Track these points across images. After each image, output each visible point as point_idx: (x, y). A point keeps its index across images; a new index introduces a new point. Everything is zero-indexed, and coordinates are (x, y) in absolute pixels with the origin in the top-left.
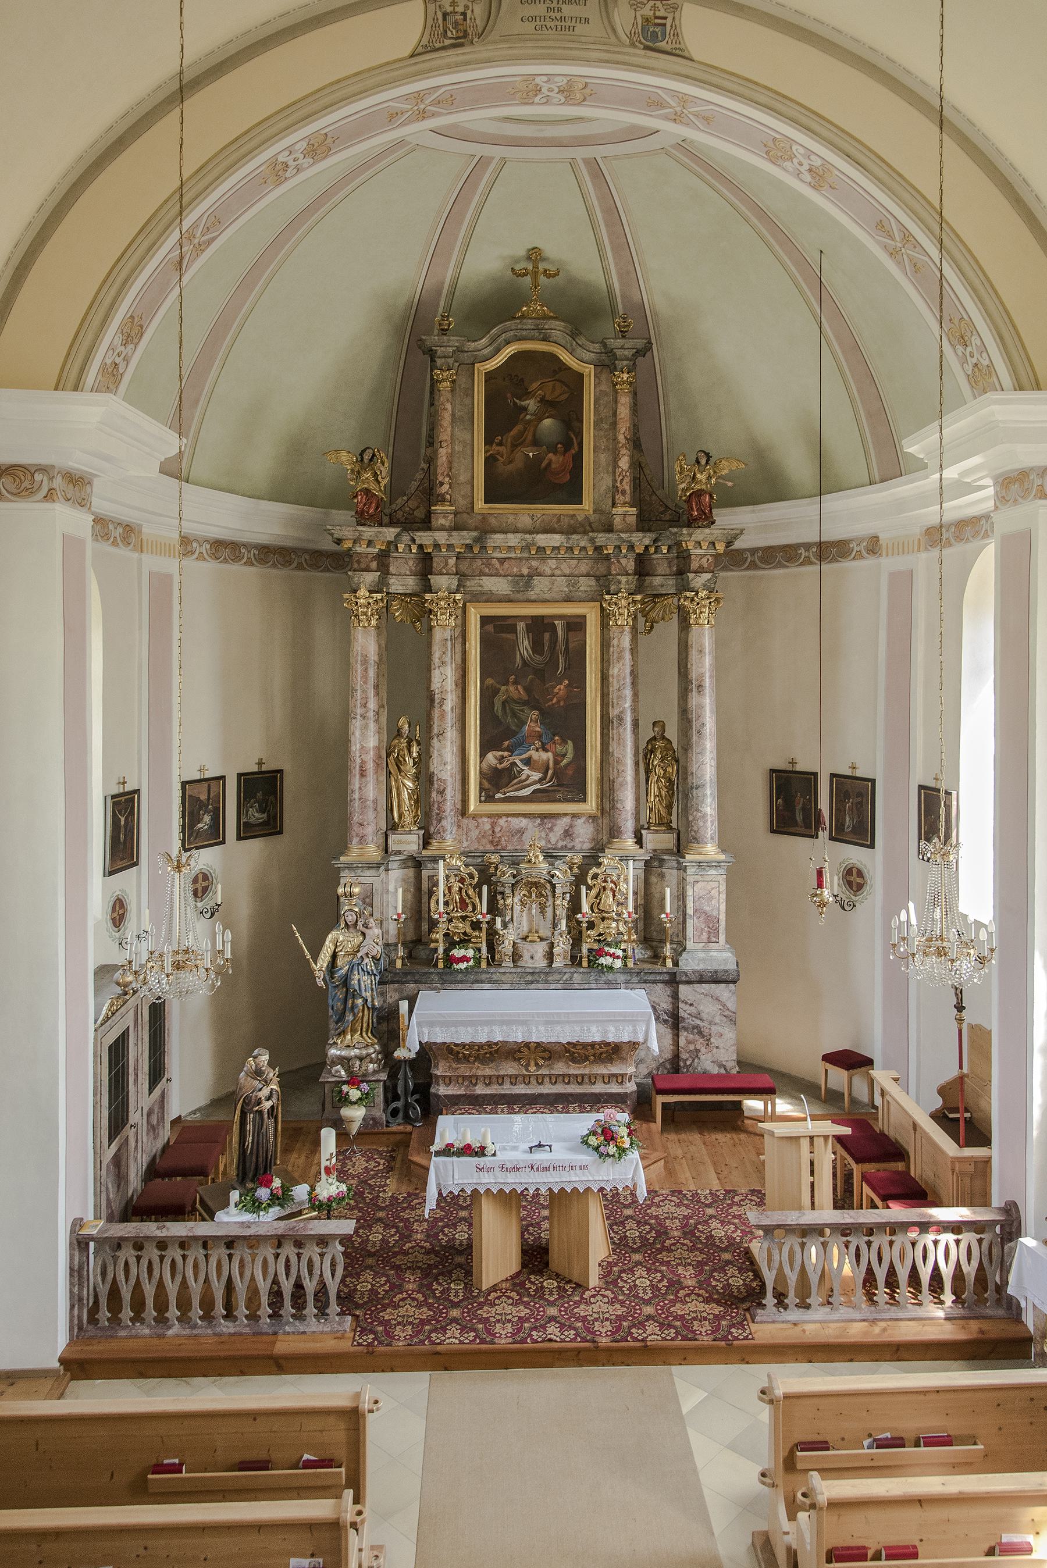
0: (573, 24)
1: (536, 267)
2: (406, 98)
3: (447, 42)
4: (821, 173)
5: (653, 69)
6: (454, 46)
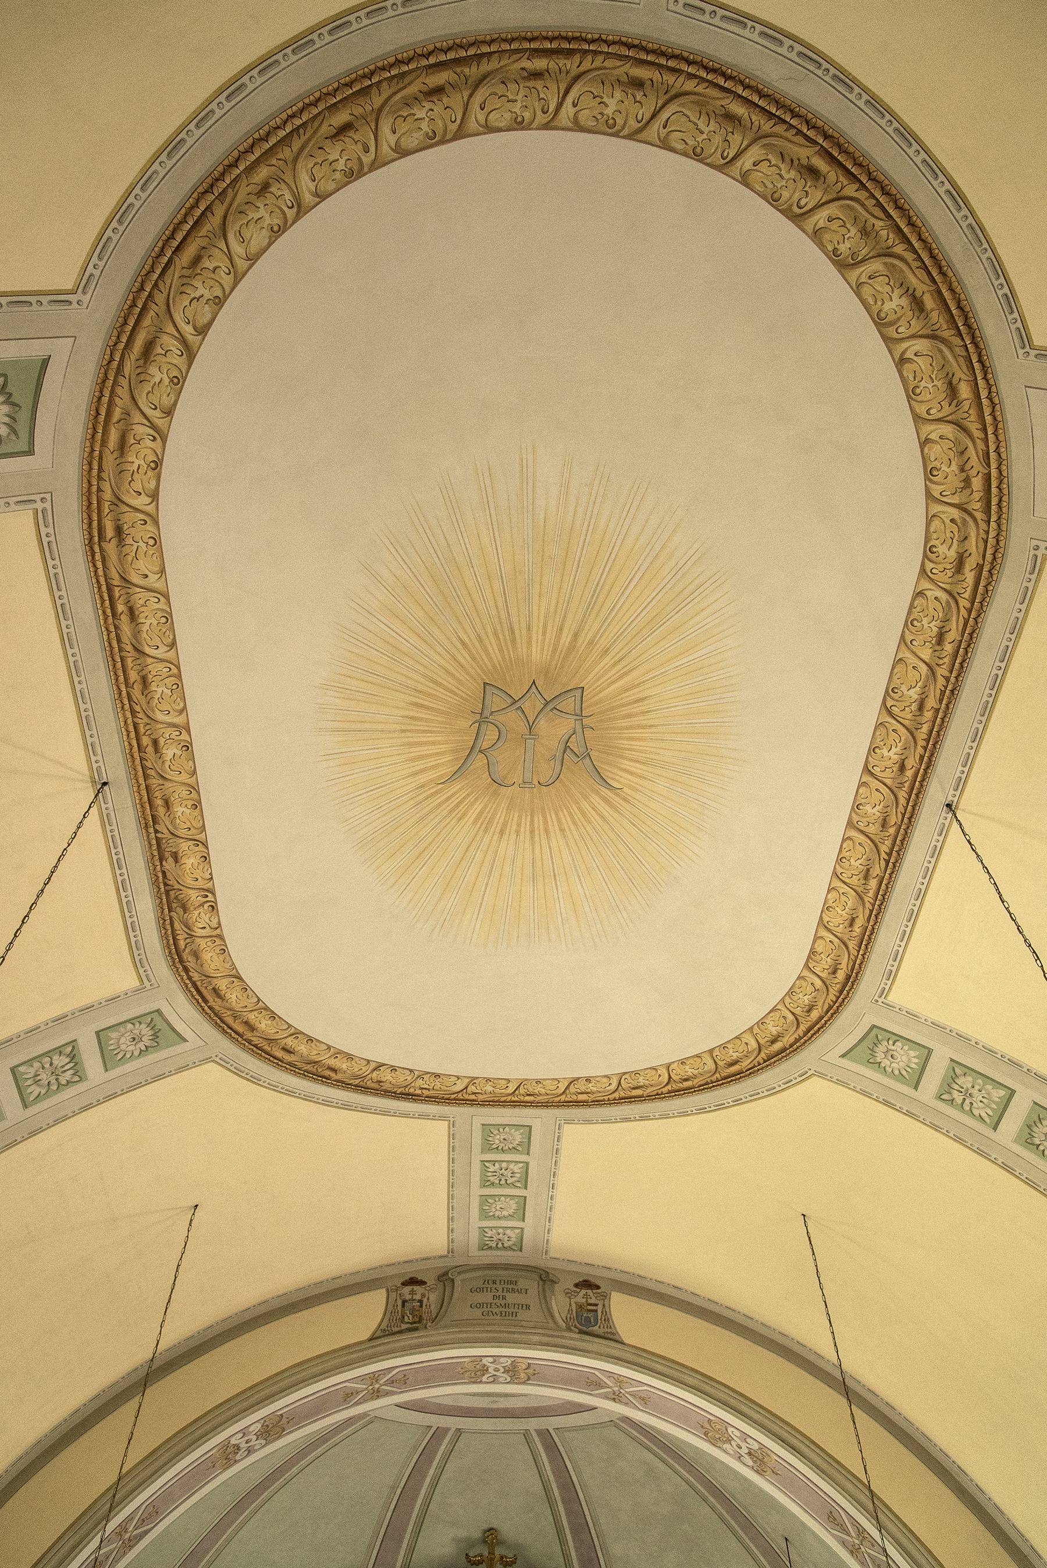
0: (516, 1310)
1: (492, 1553)
2: (362, 1378)
3: (404, 1326)
4: (761, 1457)
5: (588, 1352)
6: (409, 1330)
